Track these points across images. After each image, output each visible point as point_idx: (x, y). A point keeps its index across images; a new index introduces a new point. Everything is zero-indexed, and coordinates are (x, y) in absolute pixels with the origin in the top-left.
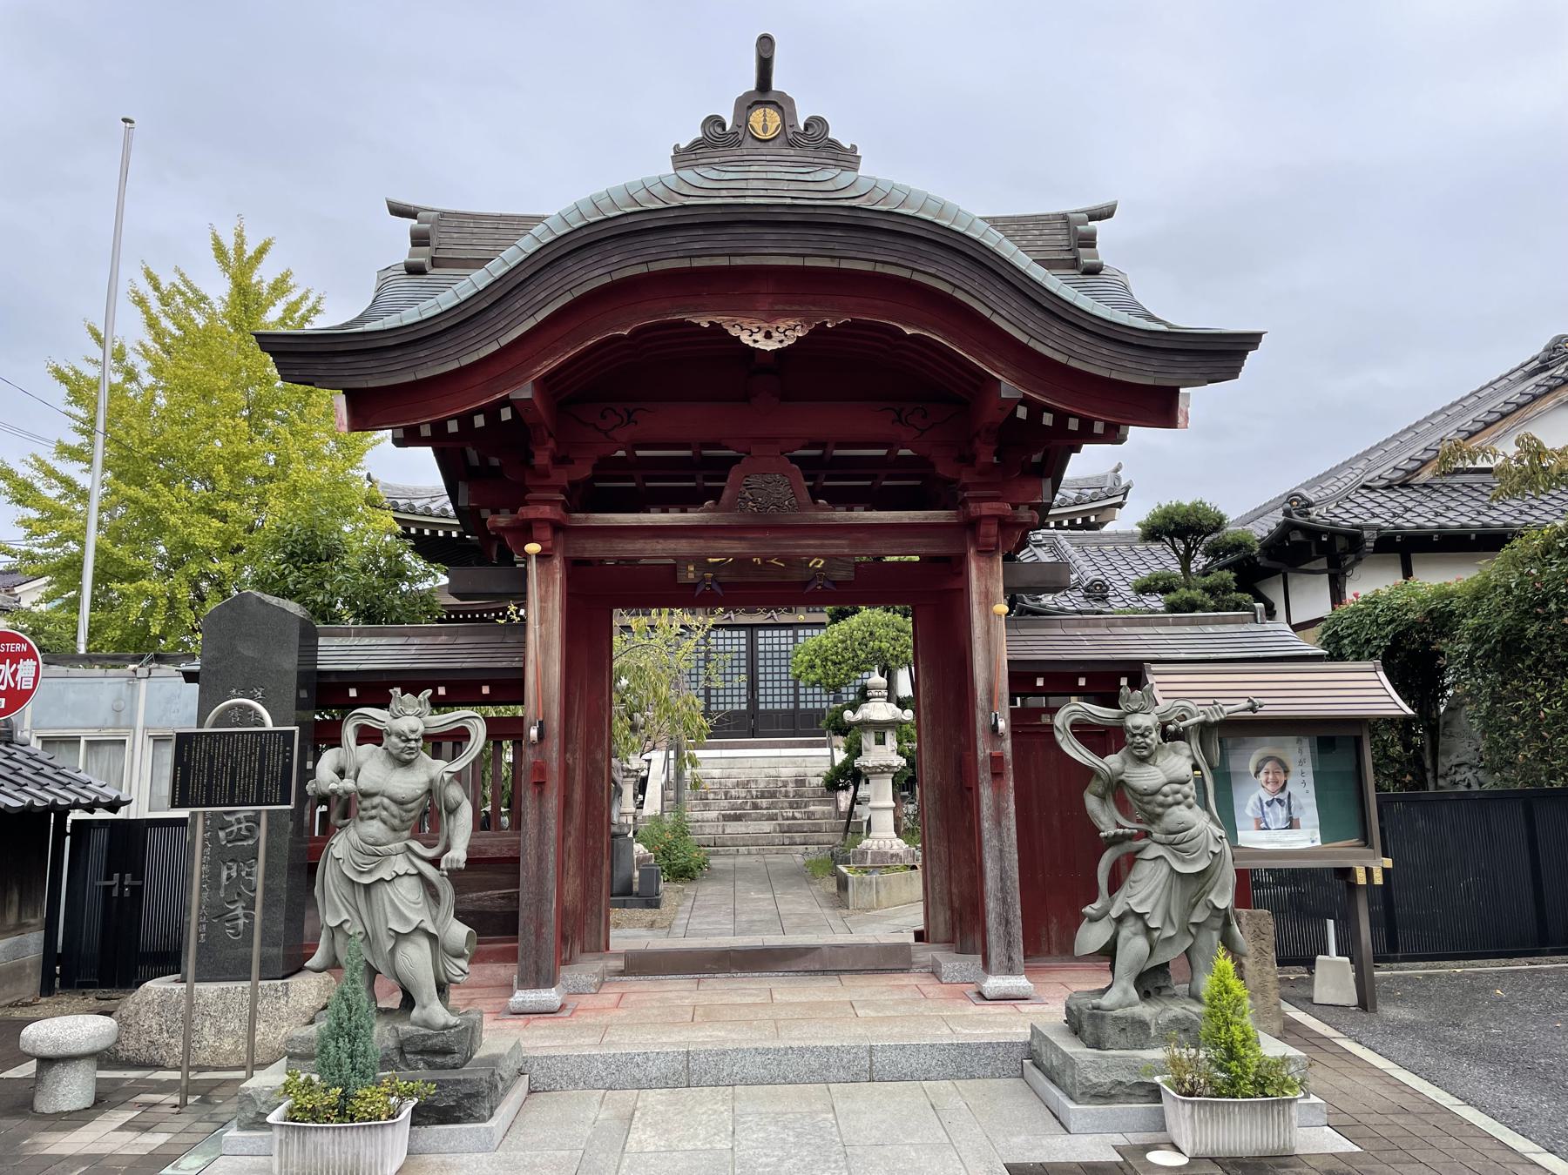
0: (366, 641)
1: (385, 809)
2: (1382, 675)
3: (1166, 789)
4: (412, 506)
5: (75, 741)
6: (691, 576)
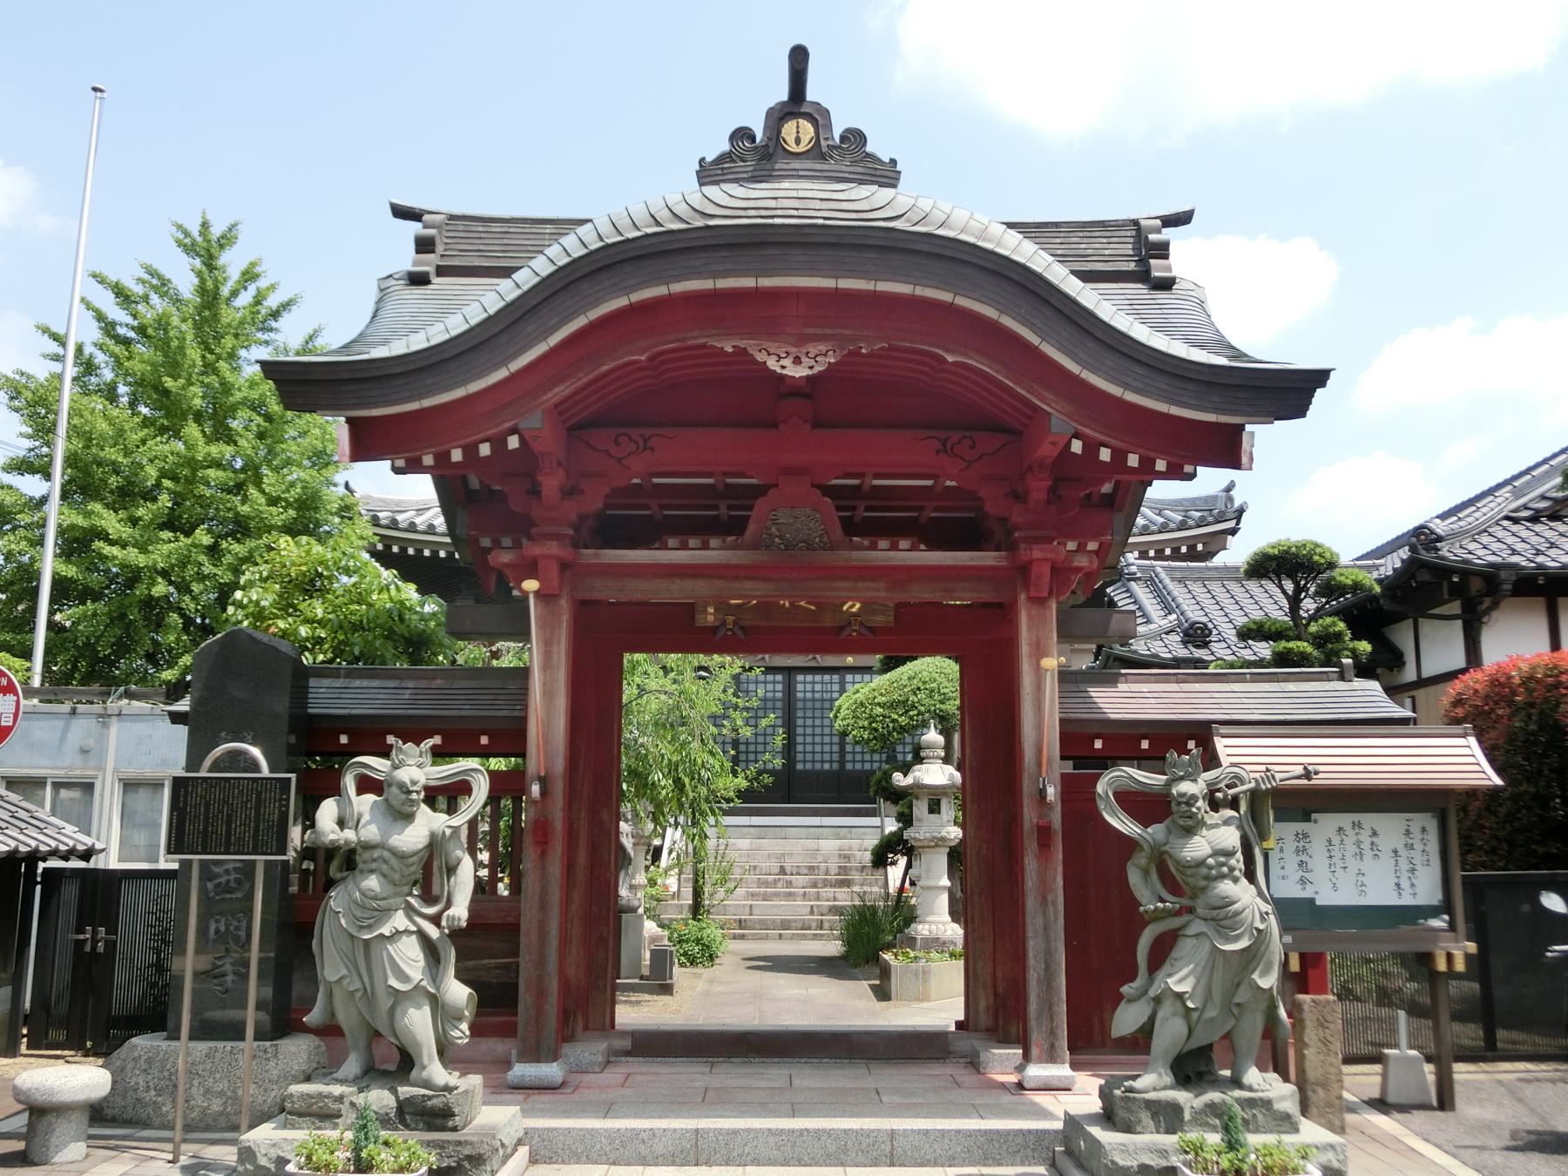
0: (357, 683)
1: (385, 862)
2: (1472, 741)
3: (1211, 861)
4: (413, 524)
5: (40, 783)
6: (711, 618)
